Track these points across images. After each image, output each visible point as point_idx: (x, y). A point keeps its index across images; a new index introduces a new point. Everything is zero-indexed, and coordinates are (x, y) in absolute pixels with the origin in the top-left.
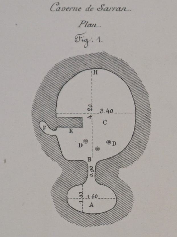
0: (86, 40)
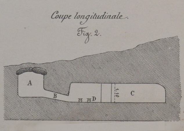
0: (87, 34)
